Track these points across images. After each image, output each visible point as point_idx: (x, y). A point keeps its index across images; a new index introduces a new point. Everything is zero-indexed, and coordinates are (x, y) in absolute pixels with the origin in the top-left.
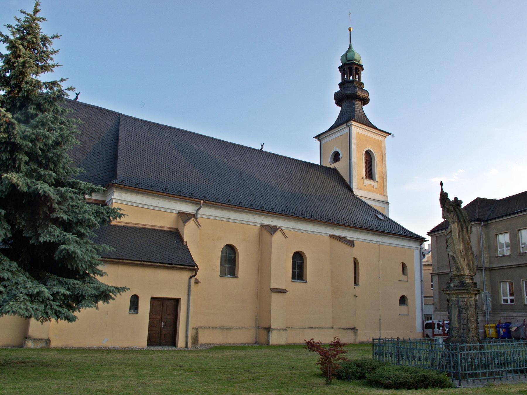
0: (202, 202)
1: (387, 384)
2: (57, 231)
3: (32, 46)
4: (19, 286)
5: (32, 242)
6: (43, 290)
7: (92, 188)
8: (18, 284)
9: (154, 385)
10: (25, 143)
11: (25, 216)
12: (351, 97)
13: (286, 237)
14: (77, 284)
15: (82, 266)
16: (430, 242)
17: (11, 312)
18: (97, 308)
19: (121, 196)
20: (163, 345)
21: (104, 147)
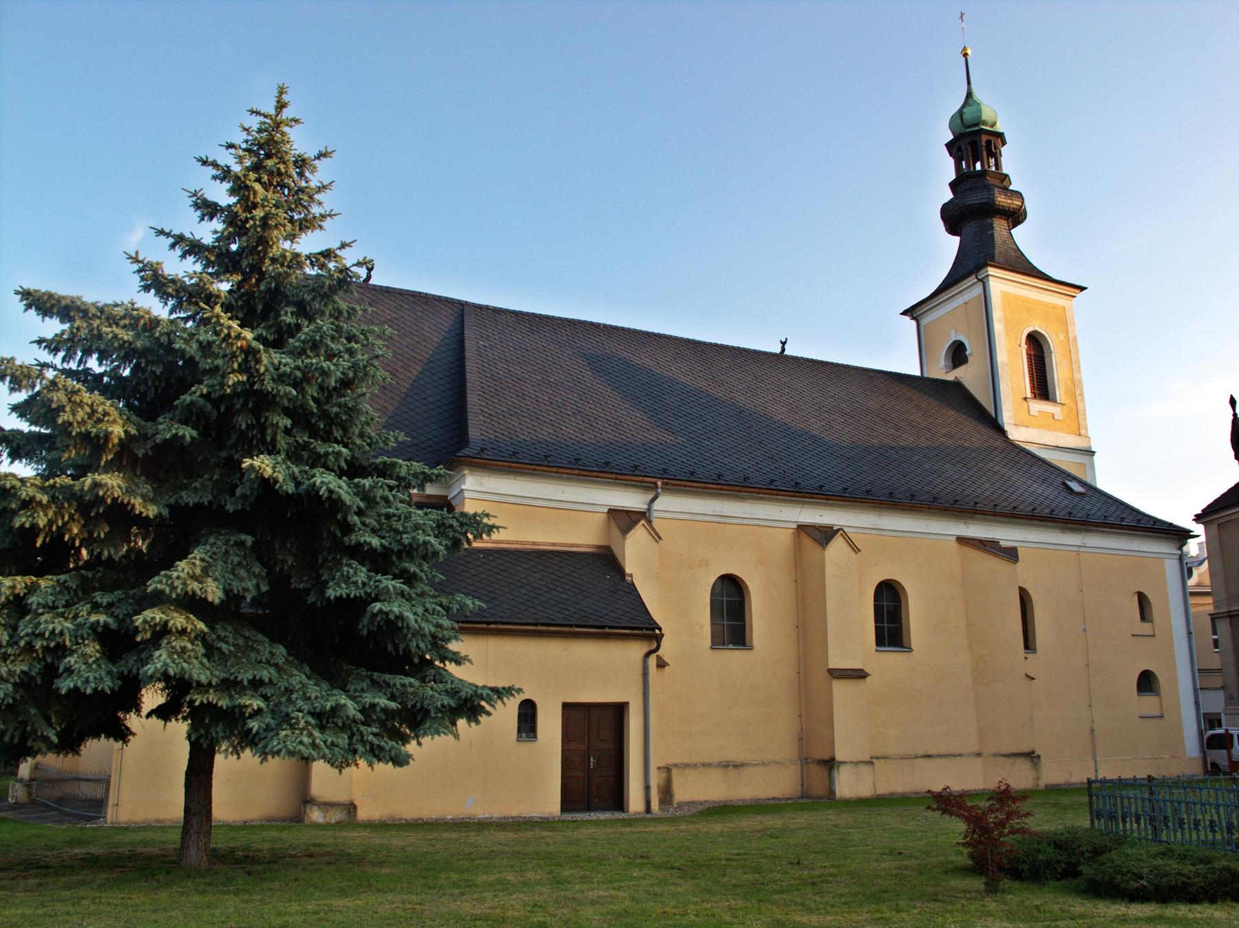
0: (659, 483)
1: (1137, 889)
2: (362, 575)
3: (277, 181)
4: (294, 696)
5: (311, 599)
6: (343, 702)
7: (423, 473)
8: (292, 692)
9: (593, 903)
10: (284, 389)
11: (292, 544)
12: (980, 211)
13: (856, 550)
14: (411, 685)
15: (418, 646)
16: (1203, 539)
17: (284, 751)
18: (457, 736)
19: (482, 484)
20: (596, 809)
21: (434, 378)
